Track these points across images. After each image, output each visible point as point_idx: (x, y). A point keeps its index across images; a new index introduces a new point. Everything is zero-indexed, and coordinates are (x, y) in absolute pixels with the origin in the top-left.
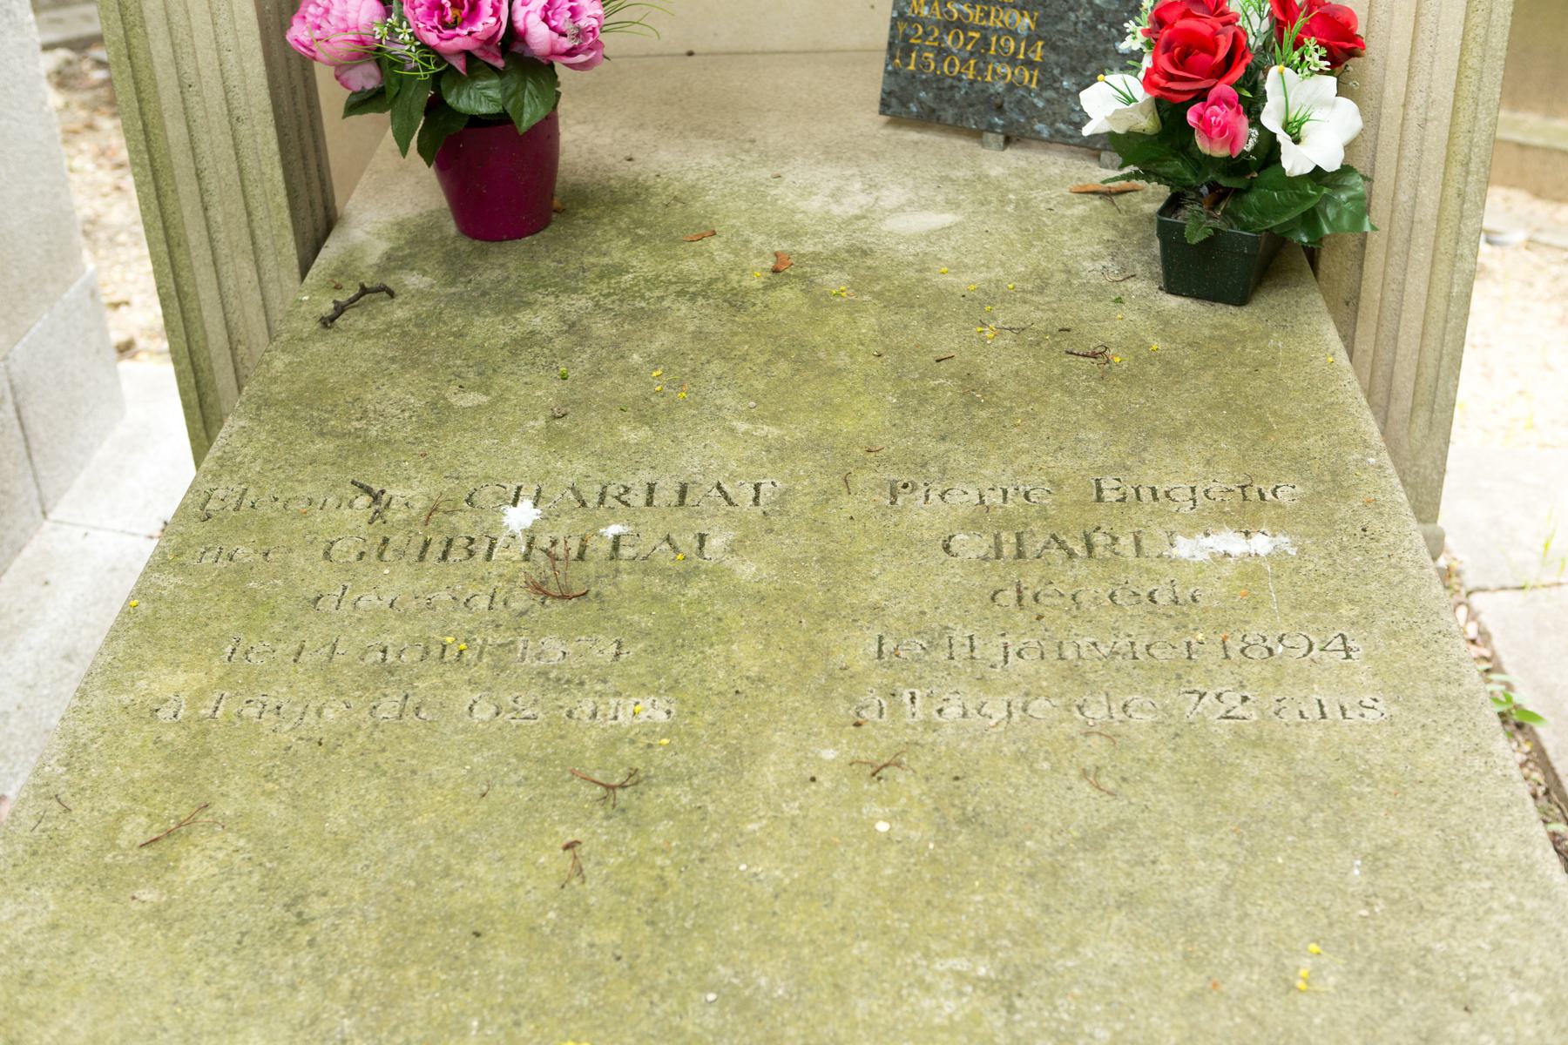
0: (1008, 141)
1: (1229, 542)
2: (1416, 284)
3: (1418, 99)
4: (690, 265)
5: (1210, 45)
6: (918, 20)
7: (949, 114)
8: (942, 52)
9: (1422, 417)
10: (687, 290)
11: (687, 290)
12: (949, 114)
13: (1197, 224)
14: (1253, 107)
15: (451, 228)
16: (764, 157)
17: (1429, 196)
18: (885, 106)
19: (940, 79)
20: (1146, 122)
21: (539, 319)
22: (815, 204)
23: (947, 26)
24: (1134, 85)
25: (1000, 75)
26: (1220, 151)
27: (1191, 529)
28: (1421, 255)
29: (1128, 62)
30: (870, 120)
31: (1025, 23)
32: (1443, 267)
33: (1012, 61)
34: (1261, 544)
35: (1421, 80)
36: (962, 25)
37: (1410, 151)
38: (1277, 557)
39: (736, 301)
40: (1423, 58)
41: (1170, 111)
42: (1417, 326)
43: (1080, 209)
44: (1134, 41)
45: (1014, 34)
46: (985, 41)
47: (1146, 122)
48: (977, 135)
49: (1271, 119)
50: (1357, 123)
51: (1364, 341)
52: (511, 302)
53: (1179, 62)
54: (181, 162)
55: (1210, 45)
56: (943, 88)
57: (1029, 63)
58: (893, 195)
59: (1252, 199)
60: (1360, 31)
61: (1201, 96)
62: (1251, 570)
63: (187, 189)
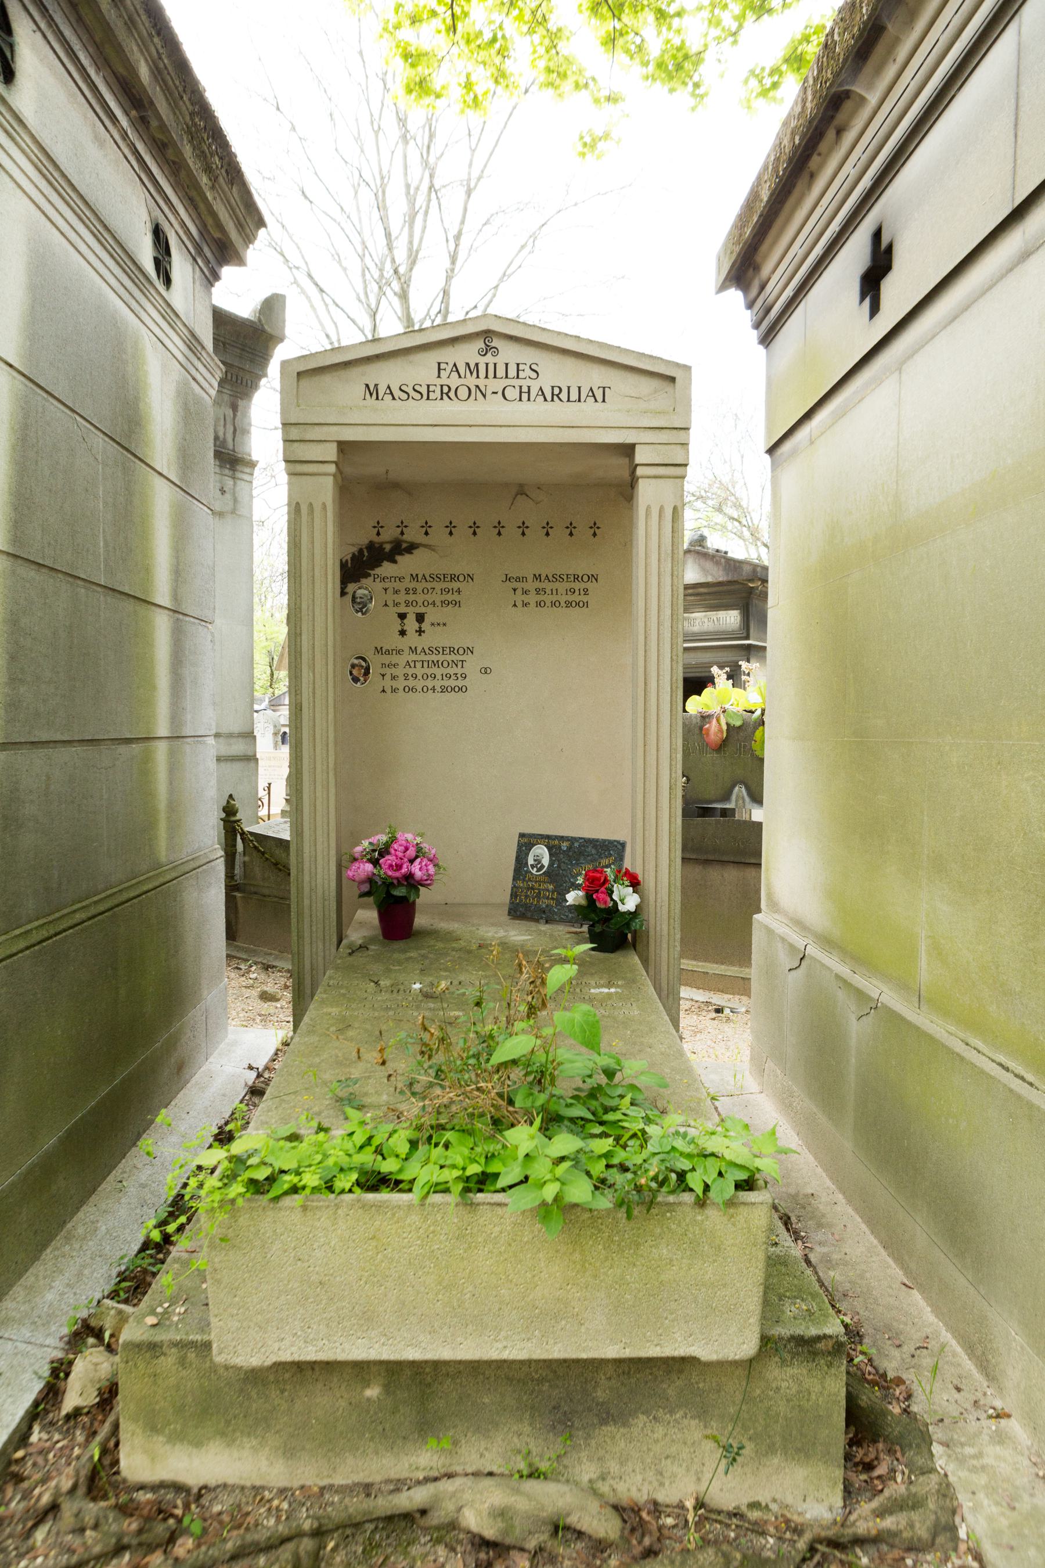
0: (547, 922)
1: (606, 990)
2: (664, 954)
3: (659, 900)
4: (454, 945)
5: (599, 879)
6: (519, 887)
7: (529, 914)
8: (527, 896)
9: (671, 997)
10: (453, 949)
11: (453, 949)
12: (529, 914)
13: (598, 929)
14: (611, 892)
15: (381, 938)
16: (473, 925)
17: (665, 927)
18: (509, 914)
19: (526, 904)
20: (584, 902)
21: (413, 954)
22: (490, 934)
23: (529, 888)
24: (581, 893)
25: (544, 903)
26: (602, 906)
27: (594, 988)
28: (665, 946)
29: (577, 887)
30: (505, 918)
31: (551, 887)
32: (671, 950)
33: (548, 898)
34: (613, 990)
35: (659, 896)
36: (533, 888)
37: (659, 915)
38: (616, 993)
39: (469, 952)
40: (659, 889)
41: (589, 897)
42: (666, 967)
43: (568, 936)
44: (580, 880)
45: (548, 890)
46: (539, 893)
47: (584, 902)
48: (537, 921)
49: (615, 897)
50: (639, 900)
51: (652, 973)
52: (404, 951)
53: (591, 883)
54: (306, 911)
55: (599, 879)
56: (527, 907)
57: (553, 899)
58: (512, 933)
59: (613, 921)
60: (640, 878)
61: (597, 891)
62: (610, 995)
63: (307, 920)
